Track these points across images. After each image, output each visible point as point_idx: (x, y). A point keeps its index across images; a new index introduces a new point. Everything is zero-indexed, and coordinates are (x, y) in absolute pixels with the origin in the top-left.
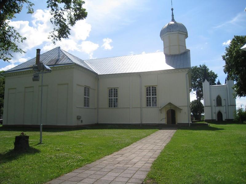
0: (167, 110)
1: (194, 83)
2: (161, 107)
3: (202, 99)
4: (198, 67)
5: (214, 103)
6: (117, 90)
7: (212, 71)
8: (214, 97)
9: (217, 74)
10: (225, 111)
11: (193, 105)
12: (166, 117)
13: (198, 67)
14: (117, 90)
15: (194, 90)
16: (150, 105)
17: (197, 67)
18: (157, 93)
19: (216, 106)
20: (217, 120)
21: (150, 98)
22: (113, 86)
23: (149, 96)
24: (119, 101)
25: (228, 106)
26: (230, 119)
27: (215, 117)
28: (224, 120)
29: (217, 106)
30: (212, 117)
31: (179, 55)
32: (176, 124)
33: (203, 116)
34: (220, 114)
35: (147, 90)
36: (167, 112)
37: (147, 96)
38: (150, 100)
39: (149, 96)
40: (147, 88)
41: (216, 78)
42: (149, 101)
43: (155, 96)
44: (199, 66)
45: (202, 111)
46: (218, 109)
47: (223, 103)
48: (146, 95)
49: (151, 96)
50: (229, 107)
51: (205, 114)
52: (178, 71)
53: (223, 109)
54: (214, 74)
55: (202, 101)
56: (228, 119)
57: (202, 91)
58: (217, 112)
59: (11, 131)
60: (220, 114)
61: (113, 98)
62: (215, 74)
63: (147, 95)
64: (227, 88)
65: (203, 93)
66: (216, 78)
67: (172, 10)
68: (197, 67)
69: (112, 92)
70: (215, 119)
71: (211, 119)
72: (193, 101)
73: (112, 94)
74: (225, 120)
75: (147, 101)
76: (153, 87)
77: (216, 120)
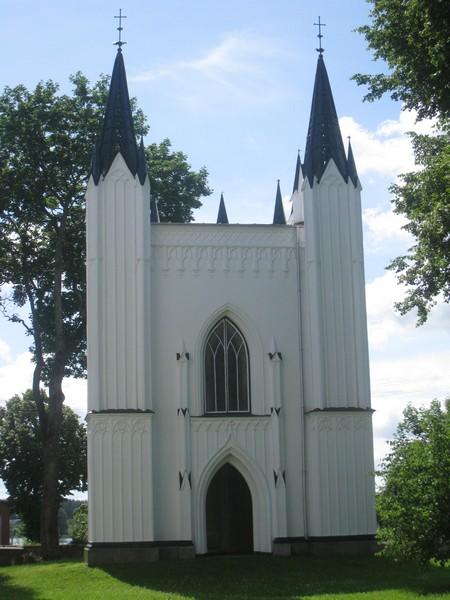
1: (24, 238)
3: (79, 375)
4: (58, 94)
5: (185, 384)
7: (167, 143)
8: (189, 334)
9: (204, 174)
10: (276, 467)
11: (12, 426)
13: (58, 94)
15: (19, 297)
17: (52, 89)
19: (197, 408)
20: (201, 547)
25: (306, 413)
26: (316, 532)
27: (186, 522)
28: (262, 542)
29: (205, 415)
30: (289, 527)
33: (82, 507)
34: (228, 493)
41: (198, 205)
44: (67, 90)
45: (76, 473)
46: (215, 441)
47: (263, 383)
50: (314, 421)
51: (93, 496)
53: (254, 445)
54: (182, 168)
55: (76, 395)
56: (299, 533)
57: (78, 302)
58: (203, 471)
60: (228, 493)
62: (194, 168)
64: (298, 250)
65: (83, 318)
66: (198, 205)
68: (52, 89)
70: (187, 537)
71: (149, 537)
72: (16, 400)
74: (278, 541)
77: (190, 544)
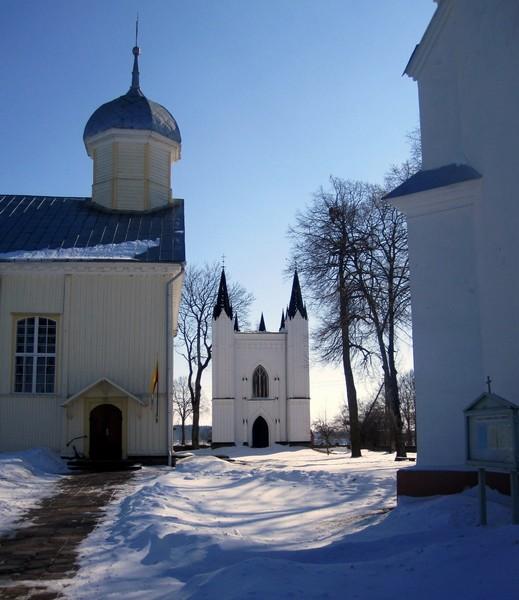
0: (93, 406)
2: (68, 397)
6: (54, 323)
12: (88, 435)
14: (54, 323)
16: (29, 389)
18: (58, 345)
21: (30, 360)
22: (40, 305)
23: (24, 354)
24: (58, 363)
31: (147, 215)
32: (124, 457)
35: (20, 331)
36: (92, 413)
37: (18, 351)
38: (30, 370)
39: (24, 354)
40: (21, 323)
42: (27, 372)
43: (50, 355)
47: (273, 387)
48: (15, 348)
49: (36, 354)
52: (141, 268)
59: (432, 469)
61: (36, 354)
63: (20, 349)
67: (136, 51)
69: (31, 331)
73: (31, 340)
75: (19, 370)
76: (42, 322)
